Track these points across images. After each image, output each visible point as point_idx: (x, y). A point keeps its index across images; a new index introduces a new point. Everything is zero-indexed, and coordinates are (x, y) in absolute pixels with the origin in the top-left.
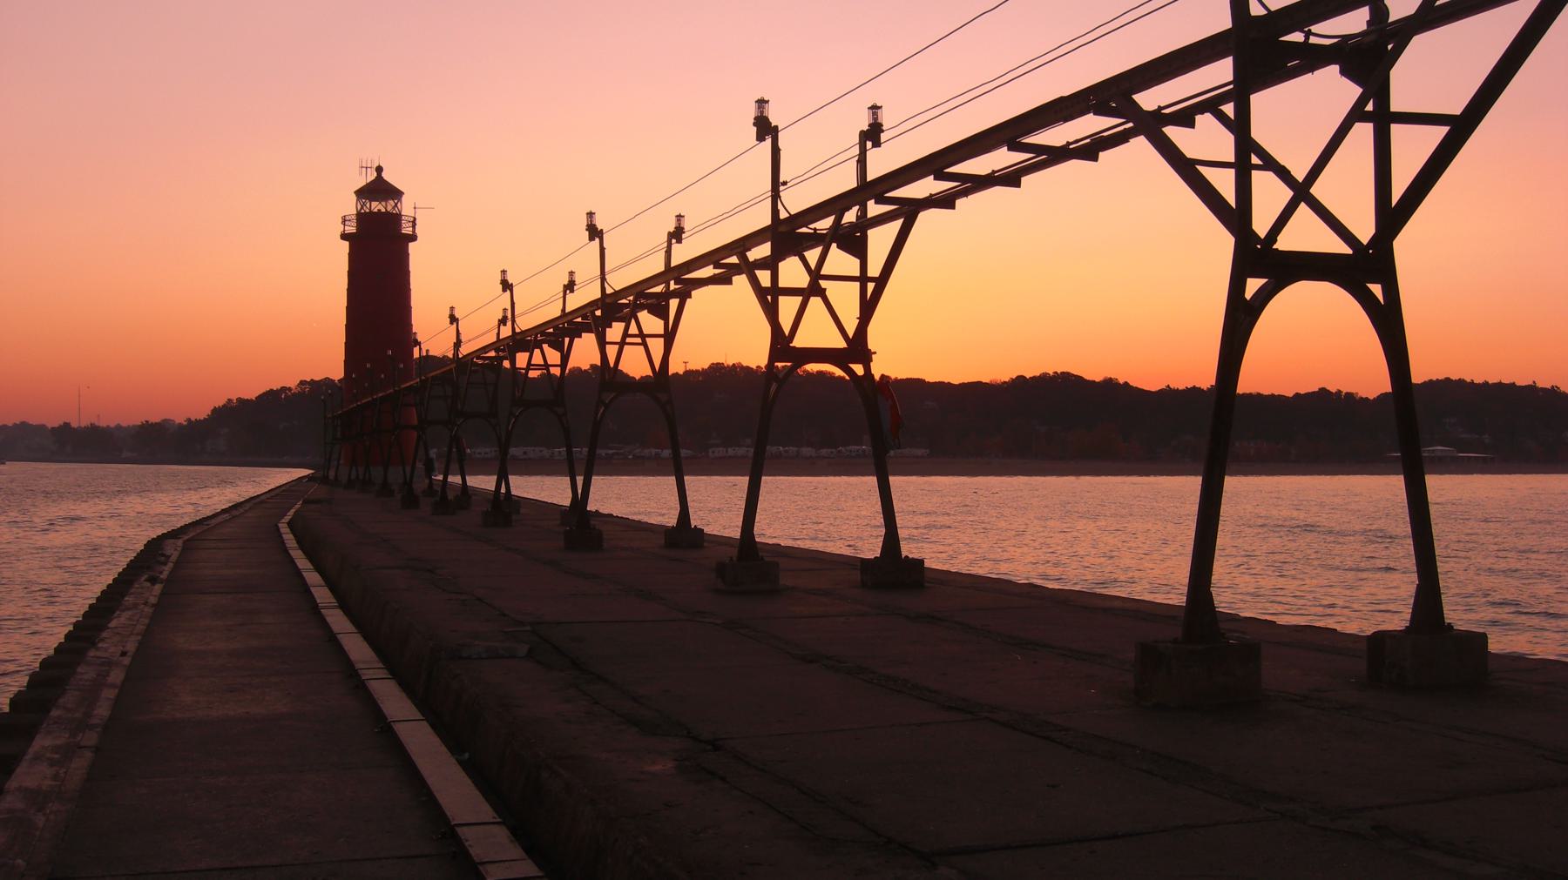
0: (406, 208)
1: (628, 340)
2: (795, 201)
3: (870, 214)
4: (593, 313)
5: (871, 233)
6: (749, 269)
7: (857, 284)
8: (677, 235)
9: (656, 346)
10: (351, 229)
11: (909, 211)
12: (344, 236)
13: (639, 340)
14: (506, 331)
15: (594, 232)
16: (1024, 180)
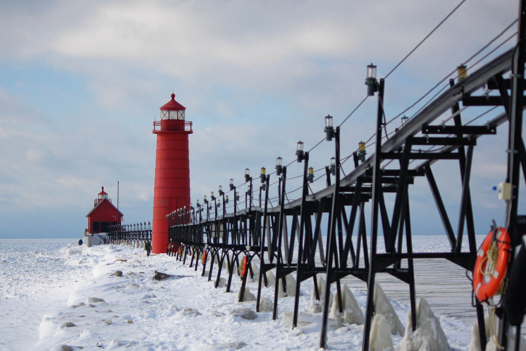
10: (159, 128)
12: (155, 132)
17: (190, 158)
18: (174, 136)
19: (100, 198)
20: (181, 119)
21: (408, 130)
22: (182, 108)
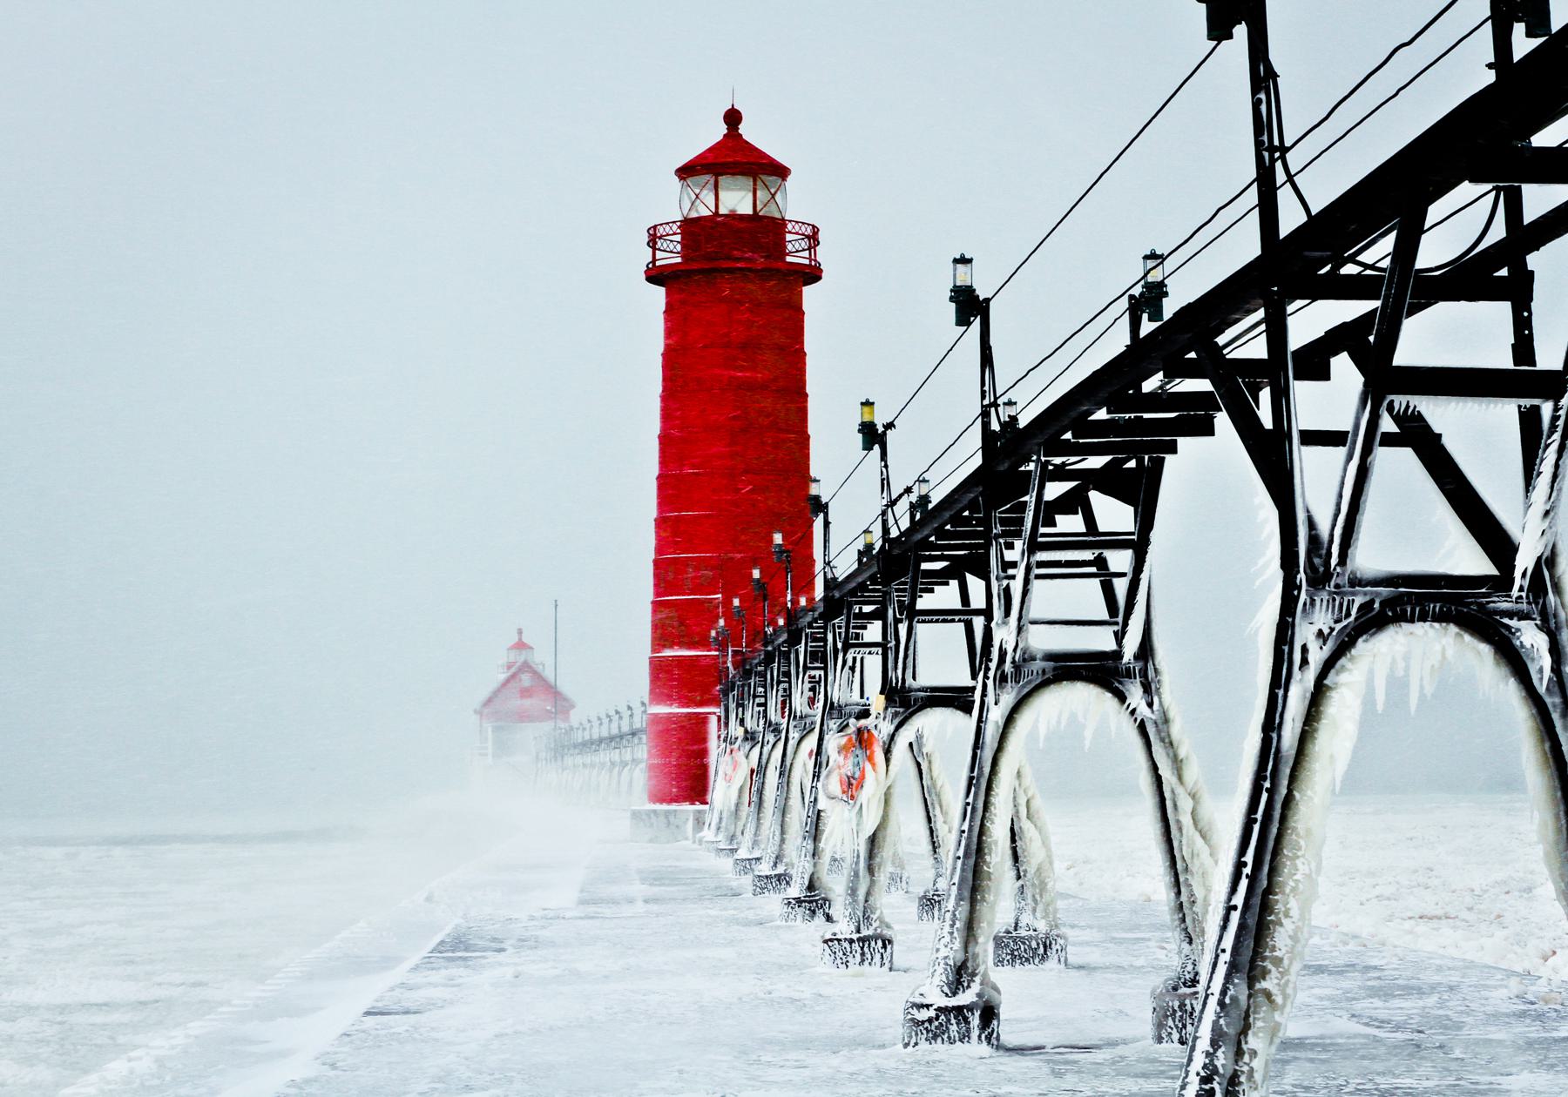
0: (796, 203)
3: (1530, 214)
10: (670, 256)
12: (655, 275)
17: (809, 344)
18: (734, 289)
19: (512, 659)
21: (1296, 544)
22: (782, 172)
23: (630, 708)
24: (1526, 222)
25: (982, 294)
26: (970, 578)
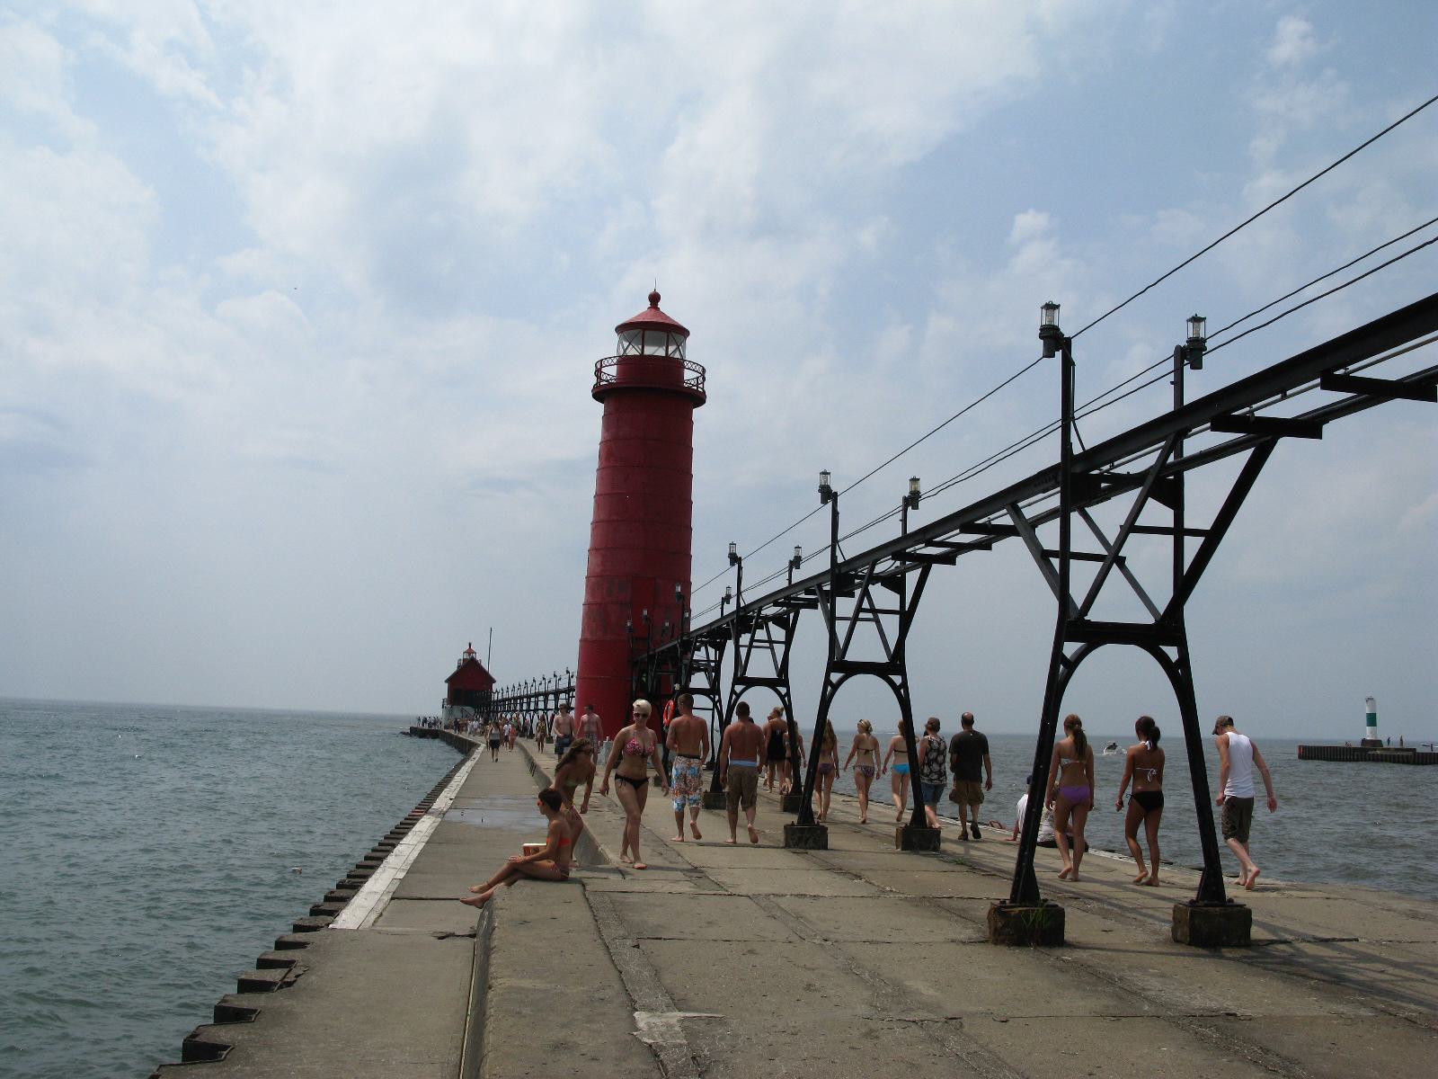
1: (862, 615)
2: (1093, 431)
4: (820, 586)
5: (1189, 476)
6: (1026, 529)
7: (1171, 538)
8: (912, 500)
9: (891, 624)
11: (1262, 437)
13: (870, 615)
14: (730, 608)
15: (828, 495)
16: (1327, 429)
20: (677, 356)
23: (526, 683)
24: (1204, 538)
25: (1067, 331)
26: (709, 648)
